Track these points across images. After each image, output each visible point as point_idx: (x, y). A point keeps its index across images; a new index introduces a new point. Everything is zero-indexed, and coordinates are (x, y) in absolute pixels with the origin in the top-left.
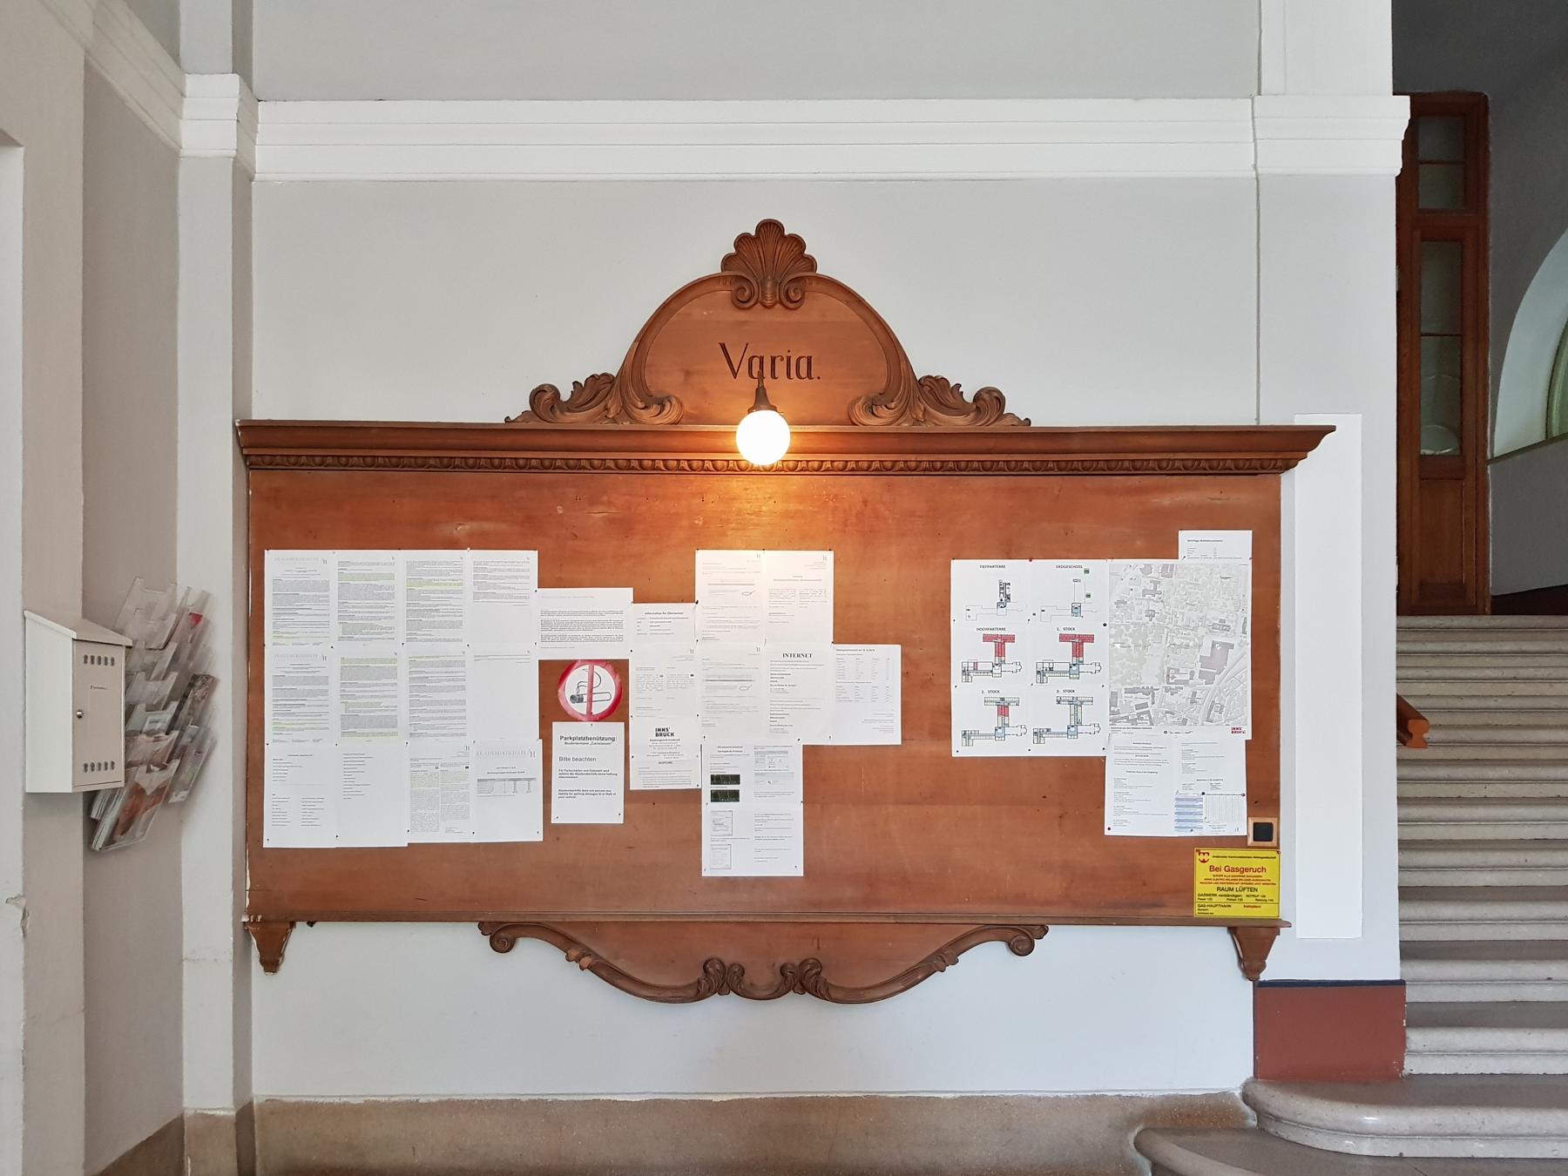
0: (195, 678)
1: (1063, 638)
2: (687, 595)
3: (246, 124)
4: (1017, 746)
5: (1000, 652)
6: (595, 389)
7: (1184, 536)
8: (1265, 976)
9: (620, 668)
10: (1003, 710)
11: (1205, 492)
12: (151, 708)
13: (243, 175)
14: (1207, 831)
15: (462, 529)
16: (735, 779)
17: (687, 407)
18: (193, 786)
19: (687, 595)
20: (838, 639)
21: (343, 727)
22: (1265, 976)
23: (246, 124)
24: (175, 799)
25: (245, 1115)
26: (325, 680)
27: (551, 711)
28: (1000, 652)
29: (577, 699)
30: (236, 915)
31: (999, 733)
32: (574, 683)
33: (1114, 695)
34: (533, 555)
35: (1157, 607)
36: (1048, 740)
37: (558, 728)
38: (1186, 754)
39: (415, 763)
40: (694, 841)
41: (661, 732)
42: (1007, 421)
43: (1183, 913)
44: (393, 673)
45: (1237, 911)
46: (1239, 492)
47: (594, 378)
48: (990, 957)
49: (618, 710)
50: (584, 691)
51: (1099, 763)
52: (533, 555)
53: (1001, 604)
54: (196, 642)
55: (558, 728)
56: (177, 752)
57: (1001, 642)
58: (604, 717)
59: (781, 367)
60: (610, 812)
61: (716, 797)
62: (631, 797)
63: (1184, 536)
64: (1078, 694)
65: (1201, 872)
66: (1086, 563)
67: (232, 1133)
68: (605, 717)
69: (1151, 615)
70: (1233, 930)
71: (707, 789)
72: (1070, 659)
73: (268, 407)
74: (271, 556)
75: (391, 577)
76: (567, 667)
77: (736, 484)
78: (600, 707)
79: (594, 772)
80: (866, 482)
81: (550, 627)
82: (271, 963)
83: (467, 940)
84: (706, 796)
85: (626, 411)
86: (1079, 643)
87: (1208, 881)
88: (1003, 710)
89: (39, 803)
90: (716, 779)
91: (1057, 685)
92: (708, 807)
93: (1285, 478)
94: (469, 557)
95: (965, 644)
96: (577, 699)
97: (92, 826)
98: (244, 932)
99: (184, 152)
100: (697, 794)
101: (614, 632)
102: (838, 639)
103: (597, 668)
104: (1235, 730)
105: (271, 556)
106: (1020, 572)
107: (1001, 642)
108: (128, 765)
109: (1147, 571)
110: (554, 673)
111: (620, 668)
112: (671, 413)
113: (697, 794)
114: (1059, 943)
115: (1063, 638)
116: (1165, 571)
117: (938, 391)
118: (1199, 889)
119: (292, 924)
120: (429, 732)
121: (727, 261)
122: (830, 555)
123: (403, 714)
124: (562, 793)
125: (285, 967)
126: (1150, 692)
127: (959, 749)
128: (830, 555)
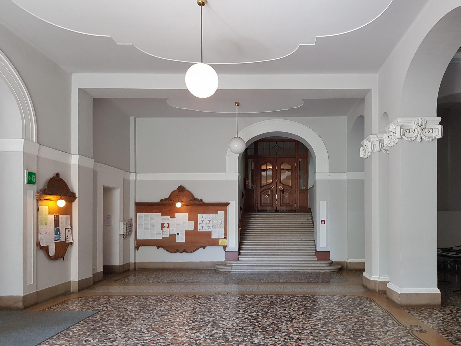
0: (131, 225)
1: (208, 221)
2: (174, 217)
3: (136, 177)
4: (204, 230)
5: (202, 222)
6: (166, 199)
7: (219, 212)
8: (226, 251)
9: (168, 224)
10: (203, 227)
11: (220, 208)
12: (128, 228)
13: (135, 181)
14: (220, 238)
15: (155, 211)
16: (179, 233)
17: (174, 201)
18: (131, 234)
19: (174, 217)
20: (188, 221)
21: (55, 228)
22: (226, 251)
23: (136, 177)
24: (130, 235)
25: (135, 263)
26: (142, 225)
27: (162, 227)
28: (202, 222)
29: (165, 226)
30: (135, 245)
31: (202, 229)
32: (165, 225)
33: (212, 226)
34: (161, 213)
35: (216, 218)
36: (200, 230)
37: (163, 229)
38: (219, 231)
39: (150, 232)
40: (175, 239)
41: (172, 229)
42: (202, 202)
43: (218, 245)
44: (148, 224)
45: (223, 245)
46: (223, 208)
47: (166, 198)
48: (202, 249)
49: (168, 227)
50: (165, 226)
51: (211, 232)
52: (161, 213)
53: (203, 218)
54: (131, 222)
55: (163, 229)
56: (130, 231)
57: (203, 221)
58: (167, 228)
59: (183, 197)
60: (168, 236)
61: (177, 235)
62: (170, 235)
63: (219, 212)
64: (209, 226)
65: (220, 241)
66: (210, 214)
67: (134, 264)
68: (167, 228)
69: (215, 219)
70: (223, 246)
71: (176, 234)
72: (202, 222)
73: (138, 201)
74: (138, 214)
75: (148, 215)
76: (164, 223)
77: (185, 201)
78: (167, 227)
79: (166, 233)
80: (191, 207)
81: (162, 220)
82: (138, 250)
83: (155, 248)
84: (176, 235)
85: (169, 201)
86: (209, 221)
87: (220, 242)
88: (203, 227)
89: (120, 235)
90: (177, 233)
91: (207, 225)
92: (176, 236)
93: (228, 206)
94: (155, 214)
95: (199, 221)
96: (165, 226)
97: (123, 237)
98: (135, 247)
99: (130, 179)
100: (175, 235)
101: (168, 220)
102: (188, 221)
103: (167, 224)
104: (223, 229)
105: (138, 214)
106: (204, 215)
107: (203, 221)
108: (126, 232)
109: (213, 215)
110: (163, 224)
111: (168, 224)
112: (173, 201)
113: (175, 235)
114: (208, 248)
115: (208, 221)
116: (217, 215)
117: (197, 200)
118: (220, 243)
119: (140, 246)
120: (222, 205)
121: (177, 189)
122: (187, 213)
123: (149, 228)
124: (163, 235)
125: (139, 250)
126: (215, 225)
127: (199, 231)
128: (187, 213)
